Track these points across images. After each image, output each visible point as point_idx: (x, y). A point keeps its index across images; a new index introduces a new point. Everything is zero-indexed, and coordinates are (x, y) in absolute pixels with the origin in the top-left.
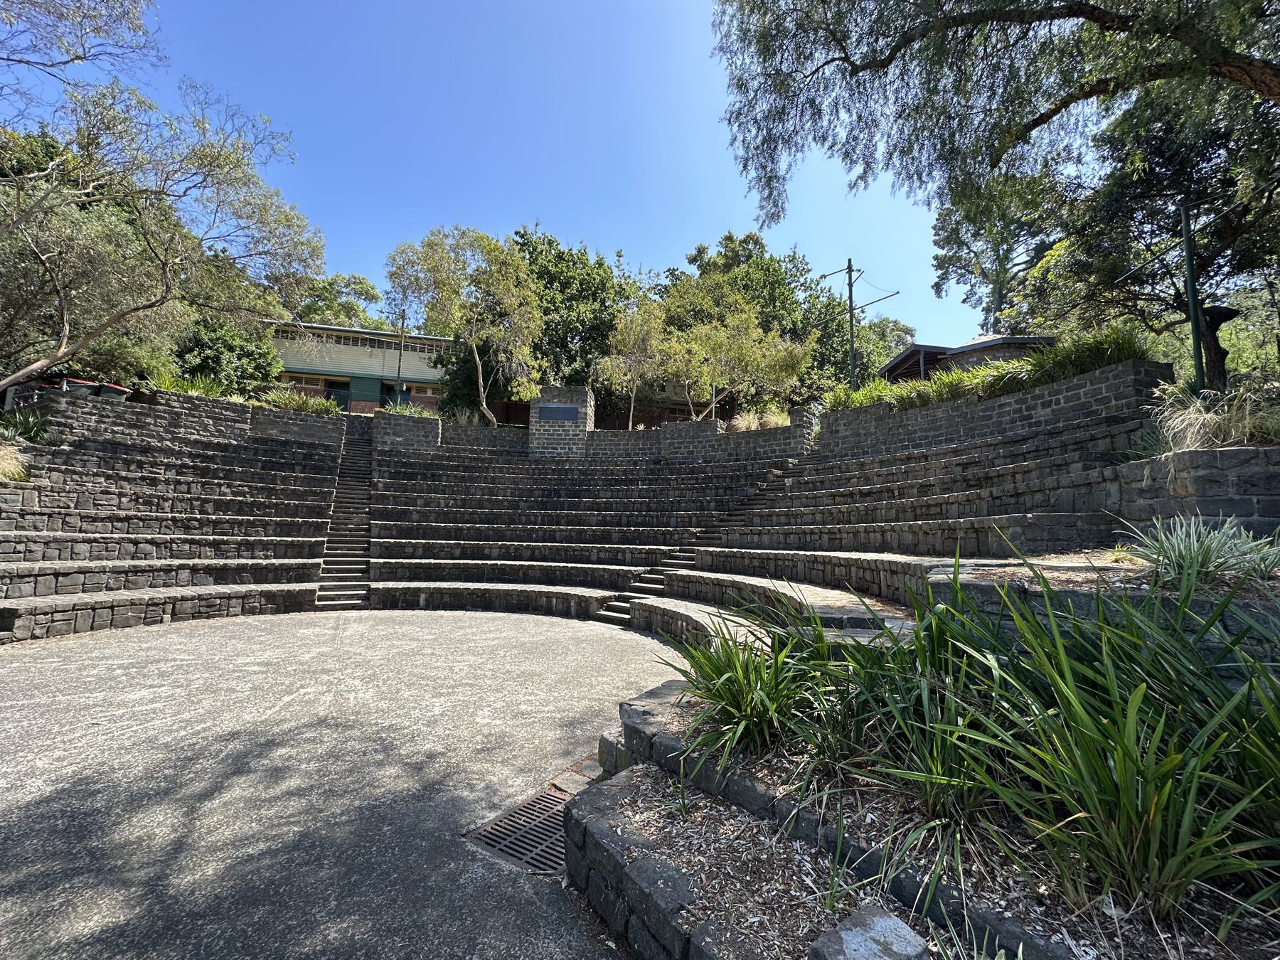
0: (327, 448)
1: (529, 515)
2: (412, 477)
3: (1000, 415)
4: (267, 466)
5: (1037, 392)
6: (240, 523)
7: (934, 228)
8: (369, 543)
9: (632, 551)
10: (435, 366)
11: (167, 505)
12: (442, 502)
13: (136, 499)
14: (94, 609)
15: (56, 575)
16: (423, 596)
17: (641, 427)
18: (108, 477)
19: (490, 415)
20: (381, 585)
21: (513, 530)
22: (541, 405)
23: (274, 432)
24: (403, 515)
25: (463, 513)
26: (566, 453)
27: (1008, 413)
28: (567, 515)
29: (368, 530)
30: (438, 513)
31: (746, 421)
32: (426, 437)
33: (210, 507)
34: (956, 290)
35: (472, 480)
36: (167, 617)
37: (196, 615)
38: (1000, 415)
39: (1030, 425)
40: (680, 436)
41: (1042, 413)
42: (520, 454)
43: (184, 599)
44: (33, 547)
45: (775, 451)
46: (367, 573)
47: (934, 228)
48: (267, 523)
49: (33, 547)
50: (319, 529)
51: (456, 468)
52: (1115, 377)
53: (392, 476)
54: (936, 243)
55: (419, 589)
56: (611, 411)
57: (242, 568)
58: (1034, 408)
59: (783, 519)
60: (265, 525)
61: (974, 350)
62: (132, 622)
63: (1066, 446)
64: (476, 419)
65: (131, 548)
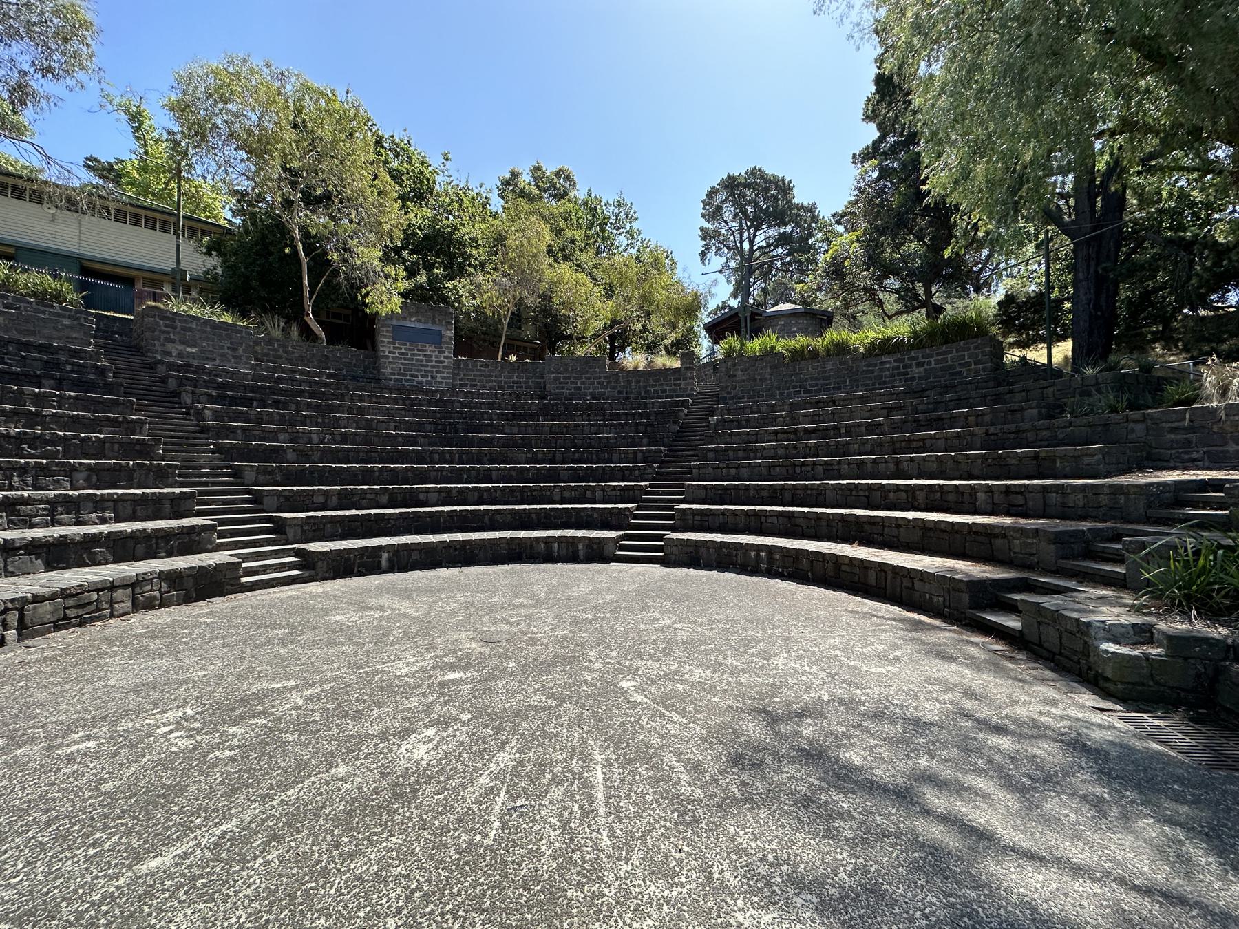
1: (443, 453)
2: (246, 402)
3: (881, 370)
5: (913, 354)
7: (703, 202)
9: (603, 489)
10: (209, 253)
12: (314, 437)
16: (385, 556)
17: (513, 359)
19: (317, 329)
21: (438, 470)
22: (395, 322)
24: (275, 454)
25: (358, 451)
26: (429, 383)
27: (888, 369)
28: (490, 453)
30: (323, 451)
31: (632, 359)
32: (235, 350)
34: (716, 261)
36: (11, 634)
38: (881, 370)
39: (906, 380)
40: (566, 370)
41: (916, 371)
42: (369, 380)
43: (37, 599)
45: (665, 391)
47: (703, 202)
48: (73, 469)
51: (300, 393)
52: (976, 348)
54: (703, 215)
55: (380, 548)
56: (476, 339)
57: (94, 540)
58: (910, 366)
59: (741, 454)
60: (70, 471)
61: (783, 316)
63: (985, 397)
64: (294, 331)
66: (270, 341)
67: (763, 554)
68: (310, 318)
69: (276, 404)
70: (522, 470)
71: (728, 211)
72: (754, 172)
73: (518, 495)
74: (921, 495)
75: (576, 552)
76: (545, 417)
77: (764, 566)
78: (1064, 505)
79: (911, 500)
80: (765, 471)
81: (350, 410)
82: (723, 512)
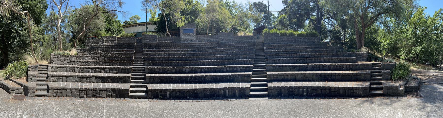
0: (132, 44)
2: (153, 48)
4: (119, 48)
6: (111, 62)
8: (144, 68)
9: (240, 67)
11: (97, 58)
13: (92, 57)
14: (71, 90)
15: (66, 77)
16: (168, 93)
18: (89, 53)
19: (169, 34)
20: (150, 75)
23: (122, 42)
24: (153, 59)
29: (144, 64)
33: (106, 59)
35: (168, 48)
36: (85, 95)
37: (93, 96)
44: (68, 69)
46: (145, 71)
49: (68, 69)
50: (130, 64)
53: (148, 49)
59: (274, 56)
60: (117, 63)
62: (76, 96)
64: (165, 35)
65: (86, 69)
66: (161, 37)
67: (305, 90)
68: (168, 31)
69: (158, 48)
70: (213, 62)
71: (254, 10)
72: (260, 2)
73: (213, 69)
74: (332, 67)
75: (235, 93)
76: (219, 47)
77: (305, 94)
78: (359, 68)
79: (329, 68)
80: (287, 61)
81: (172, 48)
82: (283, 75)
